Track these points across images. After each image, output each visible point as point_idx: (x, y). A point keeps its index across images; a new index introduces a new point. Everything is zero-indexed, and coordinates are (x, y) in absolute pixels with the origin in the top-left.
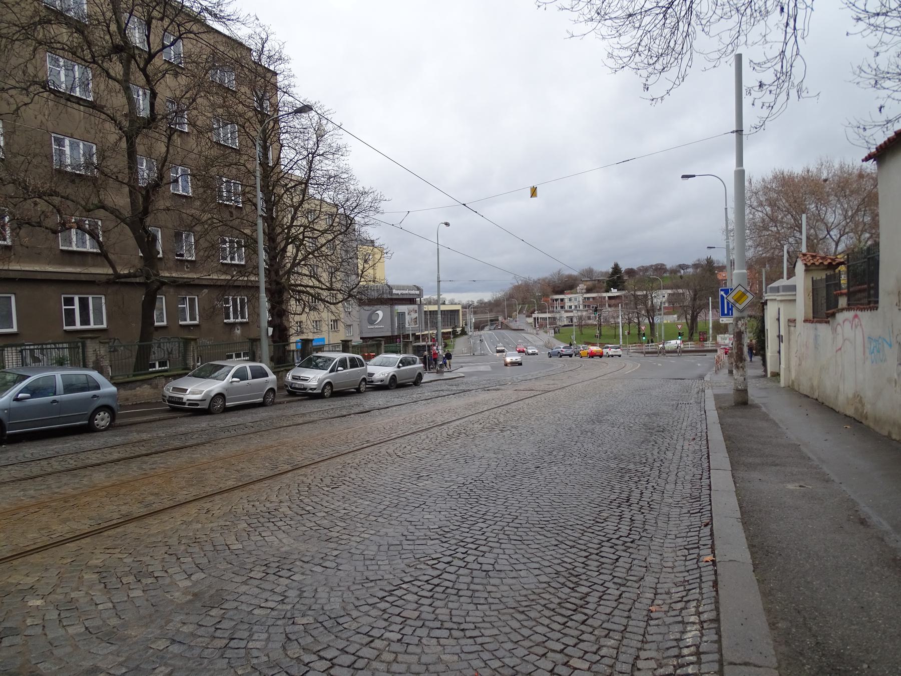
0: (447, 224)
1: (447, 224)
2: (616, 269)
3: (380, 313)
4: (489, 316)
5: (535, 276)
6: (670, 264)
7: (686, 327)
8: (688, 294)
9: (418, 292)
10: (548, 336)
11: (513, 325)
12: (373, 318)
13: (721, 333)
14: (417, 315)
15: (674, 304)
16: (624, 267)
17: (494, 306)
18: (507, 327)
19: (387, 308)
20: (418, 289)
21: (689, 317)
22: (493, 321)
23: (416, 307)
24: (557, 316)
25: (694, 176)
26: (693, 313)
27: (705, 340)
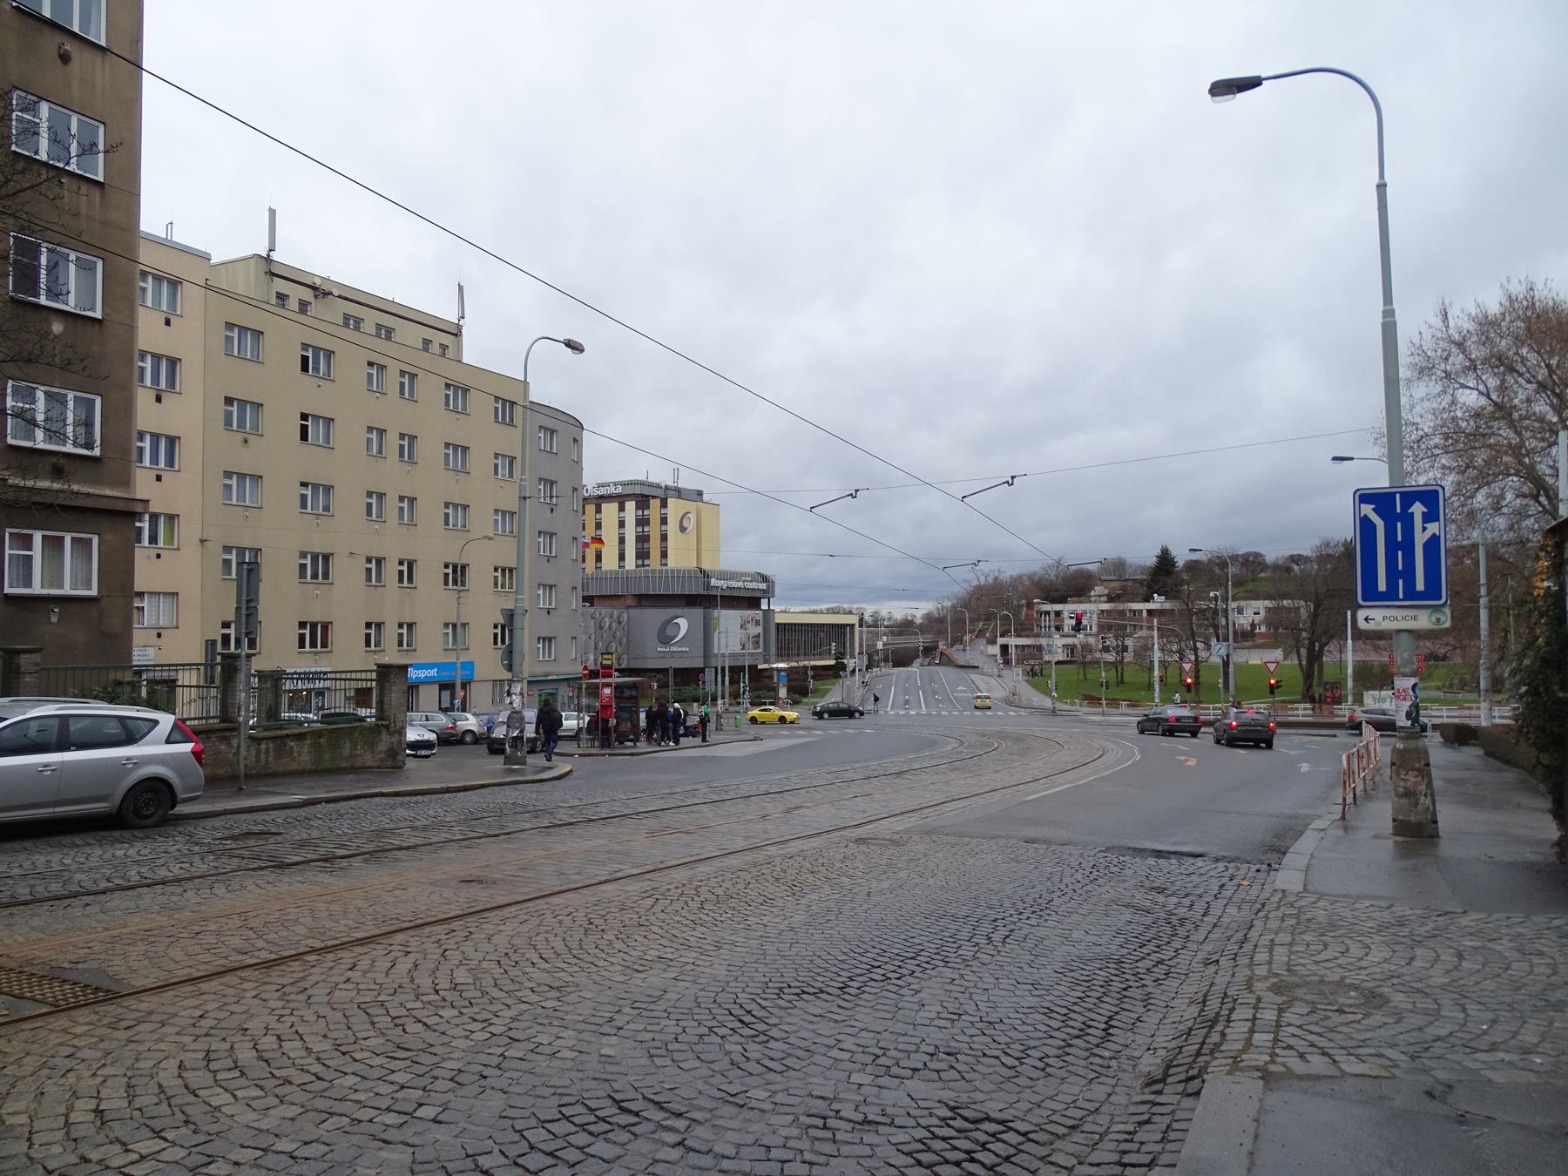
0: (573, 346)
1: (573, 346)
2: (1165, 560)
3: (683, 623)
4: (921, 641)
5: (1010, 571)
6: (1272, 554)
7: (1299, 673)
8: (1304, 609)
9: (763, 586)
10: (1015, 677)
11: (961, 658)
12: (669, 632)
13: (1374, 688)
14: (759, 630)
15: (1280, 630)
16: (1181, 557)
17: (934, 624)
18: (947, 661)
19: (698, 612)
20: (765, 579)
21: (1303, 652)
22: (929, 651)
23: (758, 614)
24: (1043, 641)
25: (1253, 83)
26: (1312, 644)
27: (1338, 701)
